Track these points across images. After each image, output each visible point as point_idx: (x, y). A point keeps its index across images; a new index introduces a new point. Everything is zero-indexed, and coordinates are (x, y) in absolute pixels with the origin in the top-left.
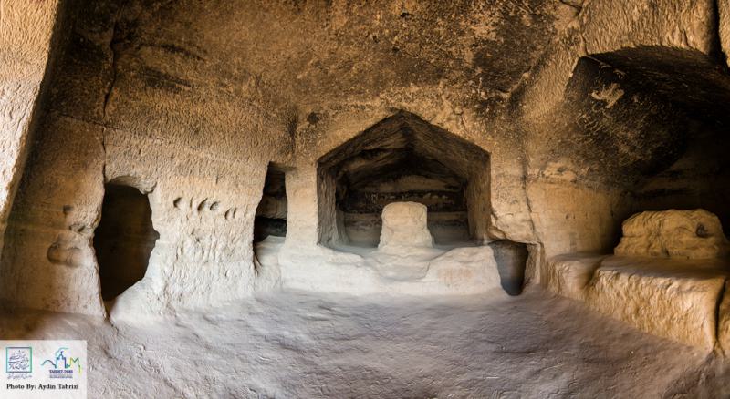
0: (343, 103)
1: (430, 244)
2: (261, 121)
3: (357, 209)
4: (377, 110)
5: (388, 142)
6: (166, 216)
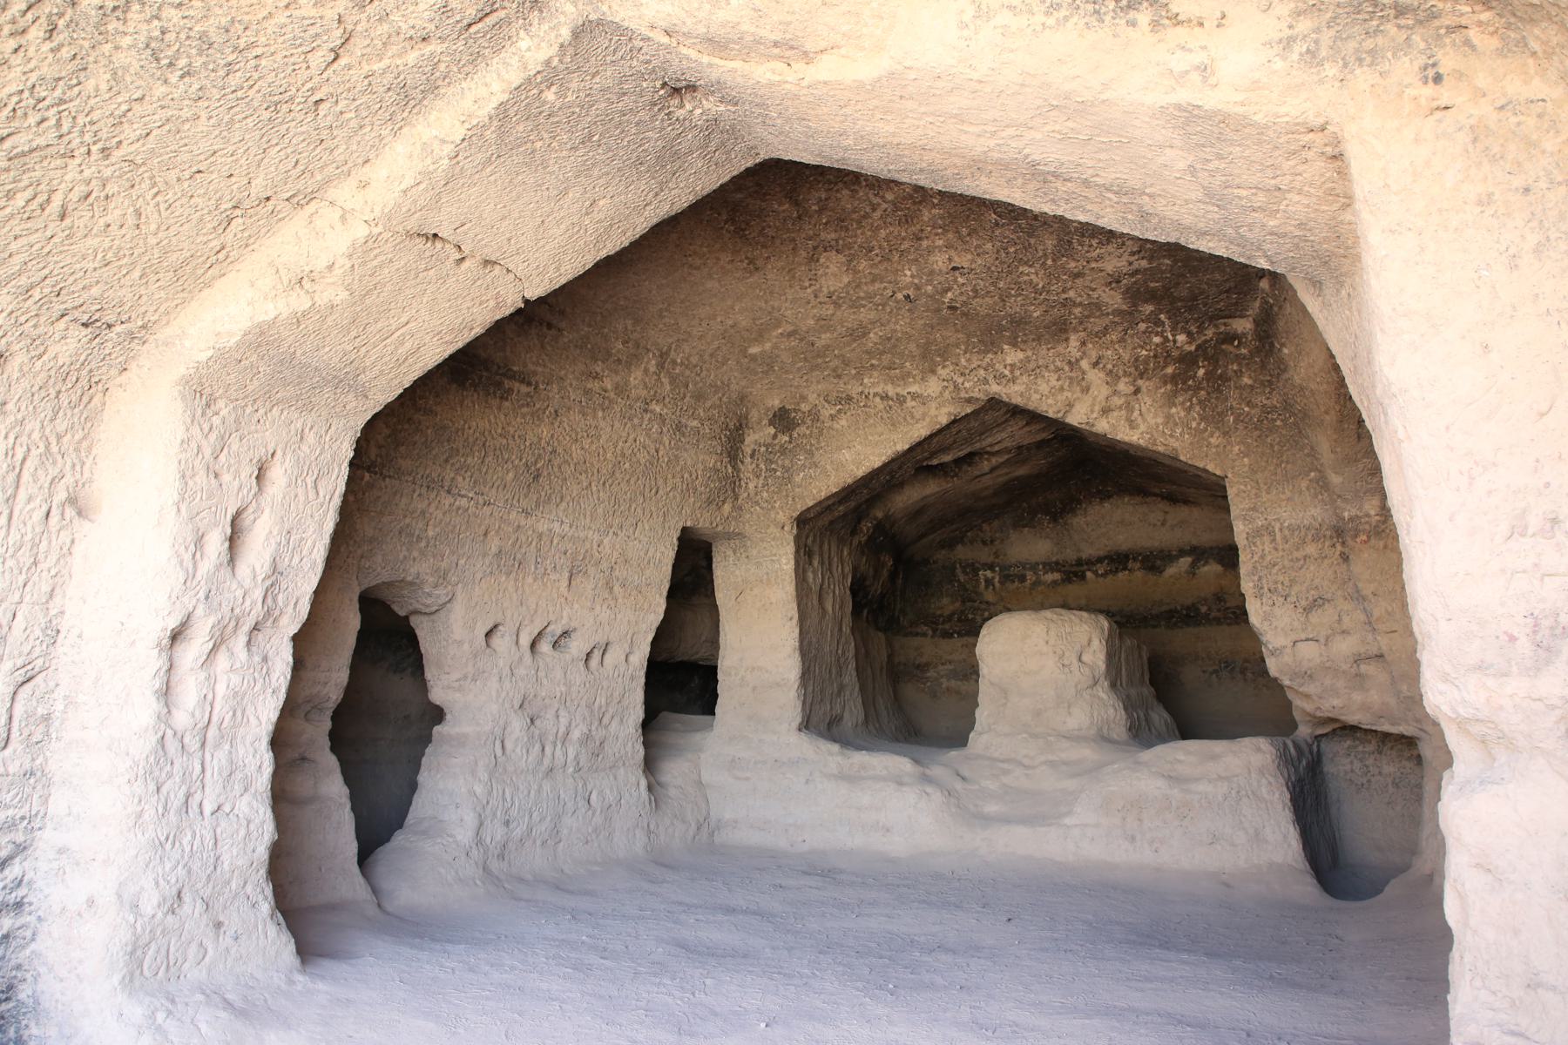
0: (854, 389)
1: (1120, 731)
2: (666, 440)
3: (933, 621)
4: (933, 405)
5: (999, 437)
6: (470, 669)
